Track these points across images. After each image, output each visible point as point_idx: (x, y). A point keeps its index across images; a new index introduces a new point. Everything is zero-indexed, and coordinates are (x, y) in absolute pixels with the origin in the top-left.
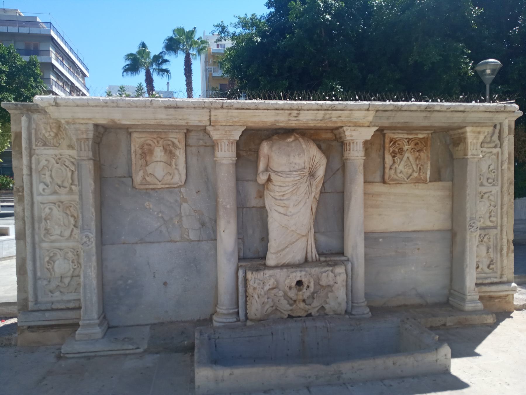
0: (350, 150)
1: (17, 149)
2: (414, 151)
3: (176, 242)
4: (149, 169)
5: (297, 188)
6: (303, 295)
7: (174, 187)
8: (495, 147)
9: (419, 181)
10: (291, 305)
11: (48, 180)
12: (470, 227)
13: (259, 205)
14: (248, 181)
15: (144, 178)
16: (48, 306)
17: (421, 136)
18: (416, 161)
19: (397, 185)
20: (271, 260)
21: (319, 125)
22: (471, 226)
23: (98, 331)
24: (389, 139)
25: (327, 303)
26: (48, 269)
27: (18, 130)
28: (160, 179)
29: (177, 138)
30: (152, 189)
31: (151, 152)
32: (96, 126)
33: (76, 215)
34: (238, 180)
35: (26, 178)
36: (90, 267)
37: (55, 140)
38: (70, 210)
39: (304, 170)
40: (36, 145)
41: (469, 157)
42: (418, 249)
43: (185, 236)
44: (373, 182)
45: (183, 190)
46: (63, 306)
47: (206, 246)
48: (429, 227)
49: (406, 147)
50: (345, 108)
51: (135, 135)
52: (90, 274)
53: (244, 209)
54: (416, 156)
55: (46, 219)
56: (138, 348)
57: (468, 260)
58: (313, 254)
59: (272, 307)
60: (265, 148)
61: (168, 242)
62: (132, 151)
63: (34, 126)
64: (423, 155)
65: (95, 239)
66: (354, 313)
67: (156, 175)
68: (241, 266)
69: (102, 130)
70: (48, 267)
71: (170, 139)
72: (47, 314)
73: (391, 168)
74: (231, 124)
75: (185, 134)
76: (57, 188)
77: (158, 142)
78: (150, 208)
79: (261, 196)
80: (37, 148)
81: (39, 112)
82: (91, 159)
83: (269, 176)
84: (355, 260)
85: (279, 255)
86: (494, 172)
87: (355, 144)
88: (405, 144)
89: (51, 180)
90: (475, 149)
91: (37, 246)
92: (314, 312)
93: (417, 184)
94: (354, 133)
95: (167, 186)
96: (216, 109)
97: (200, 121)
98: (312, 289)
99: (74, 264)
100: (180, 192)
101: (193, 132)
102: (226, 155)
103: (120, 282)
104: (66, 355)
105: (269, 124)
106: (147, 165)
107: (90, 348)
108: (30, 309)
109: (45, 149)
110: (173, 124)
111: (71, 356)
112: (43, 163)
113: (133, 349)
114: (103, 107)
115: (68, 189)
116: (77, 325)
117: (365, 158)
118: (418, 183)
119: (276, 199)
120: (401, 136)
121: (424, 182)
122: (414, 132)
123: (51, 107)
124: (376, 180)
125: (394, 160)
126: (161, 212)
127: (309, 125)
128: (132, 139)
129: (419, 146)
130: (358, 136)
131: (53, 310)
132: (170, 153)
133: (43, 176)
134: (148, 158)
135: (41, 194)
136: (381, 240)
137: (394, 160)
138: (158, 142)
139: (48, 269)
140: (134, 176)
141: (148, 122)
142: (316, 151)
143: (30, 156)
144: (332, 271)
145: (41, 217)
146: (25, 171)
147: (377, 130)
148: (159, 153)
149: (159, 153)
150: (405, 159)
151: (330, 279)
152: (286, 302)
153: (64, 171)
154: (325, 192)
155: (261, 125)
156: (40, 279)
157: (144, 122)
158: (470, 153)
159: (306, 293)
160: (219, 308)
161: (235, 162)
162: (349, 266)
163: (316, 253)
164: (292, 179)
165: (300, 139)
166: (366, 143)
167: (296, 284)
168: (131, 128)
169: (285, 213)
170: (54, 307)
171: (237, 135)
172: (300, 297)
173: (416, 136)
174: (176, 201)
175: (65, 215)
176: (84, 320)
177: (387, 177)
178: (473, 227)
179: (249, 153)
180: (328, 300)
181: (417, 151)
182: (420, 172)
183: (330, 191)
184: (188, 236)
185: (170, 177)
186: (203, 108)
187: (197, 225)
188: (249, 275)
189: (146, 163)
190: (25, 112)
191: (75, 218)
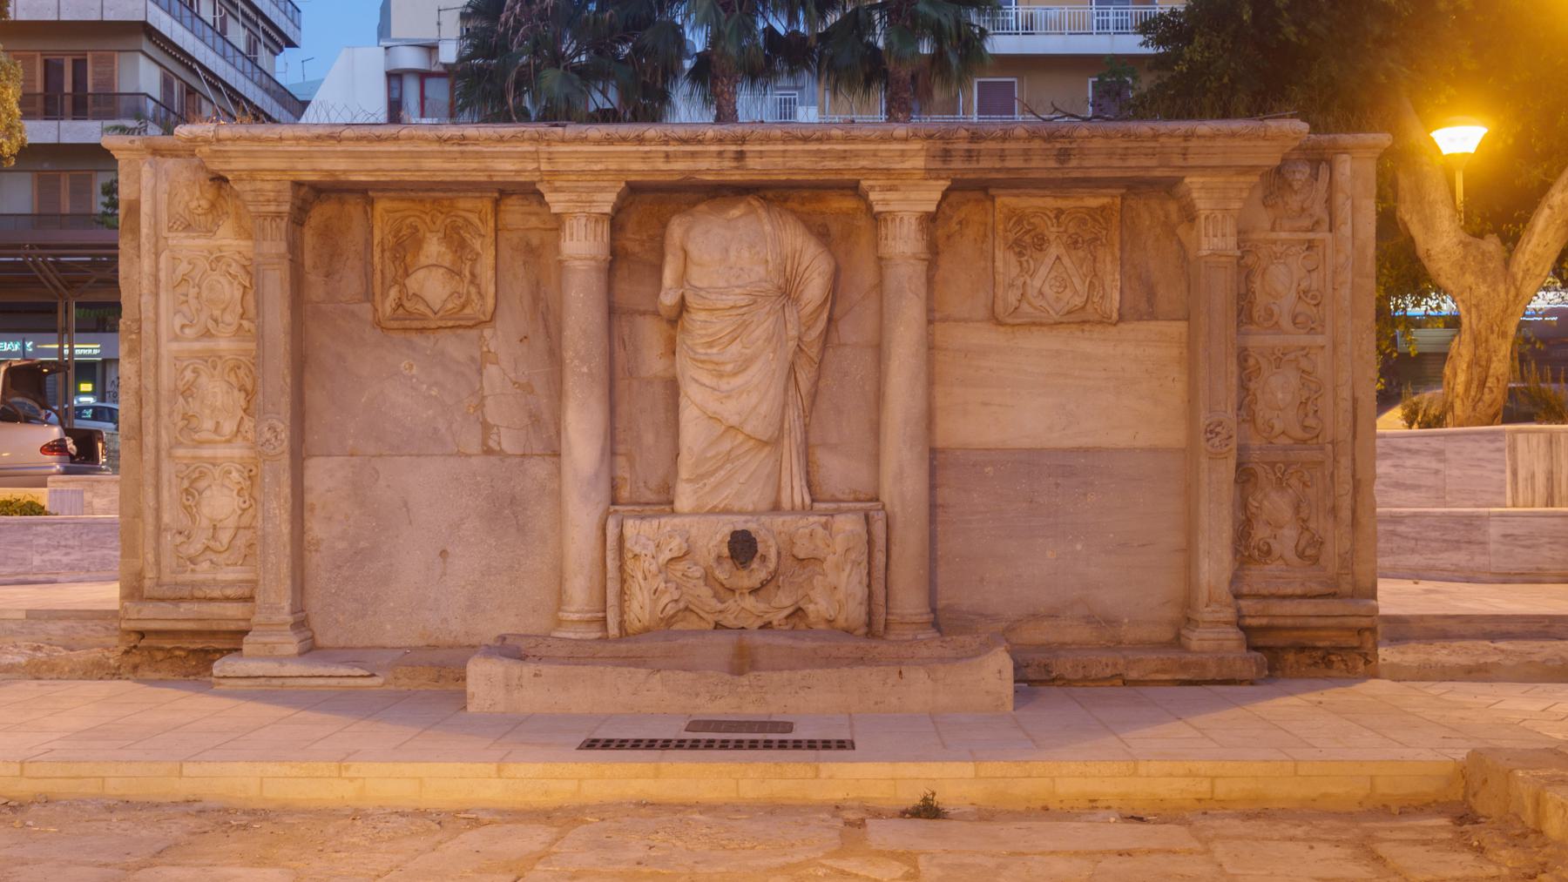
4: (413, 284)
14: (644, 313)
15: (400, 305)
19: (1034, 328)
21: (737, 178)
27: (133, 197)
28: (436, 308)
31: (418, 243)
32: (297, 184)
33: (249, 387)
34: (613, 312)
35: (146, 300)
37: (210, 217)
40: (170, 229)
44: (966, 321)
45: (487, 332)
47: (540, 469)
49: (1052, 232)
56: (373, 675)
59: (676, 601)
72: (184, 607)
91: (163, 454)
92: (777, 618)
98: (772, 565)
102: (582, 245)
103: (341, 545)
116: (246, 633)
121: (1104, 321)
125: (1021, 264)
132: (457, 241)
134: (408, 259)
135: (176, 338)
143: (157, 255)
148: (434, 248)
149: (434, 248)
151: (820, 543)
153: (227, 286)
171: (606, 202)
174: (473, 359)
177: (999, 308)
188: (631, 527)
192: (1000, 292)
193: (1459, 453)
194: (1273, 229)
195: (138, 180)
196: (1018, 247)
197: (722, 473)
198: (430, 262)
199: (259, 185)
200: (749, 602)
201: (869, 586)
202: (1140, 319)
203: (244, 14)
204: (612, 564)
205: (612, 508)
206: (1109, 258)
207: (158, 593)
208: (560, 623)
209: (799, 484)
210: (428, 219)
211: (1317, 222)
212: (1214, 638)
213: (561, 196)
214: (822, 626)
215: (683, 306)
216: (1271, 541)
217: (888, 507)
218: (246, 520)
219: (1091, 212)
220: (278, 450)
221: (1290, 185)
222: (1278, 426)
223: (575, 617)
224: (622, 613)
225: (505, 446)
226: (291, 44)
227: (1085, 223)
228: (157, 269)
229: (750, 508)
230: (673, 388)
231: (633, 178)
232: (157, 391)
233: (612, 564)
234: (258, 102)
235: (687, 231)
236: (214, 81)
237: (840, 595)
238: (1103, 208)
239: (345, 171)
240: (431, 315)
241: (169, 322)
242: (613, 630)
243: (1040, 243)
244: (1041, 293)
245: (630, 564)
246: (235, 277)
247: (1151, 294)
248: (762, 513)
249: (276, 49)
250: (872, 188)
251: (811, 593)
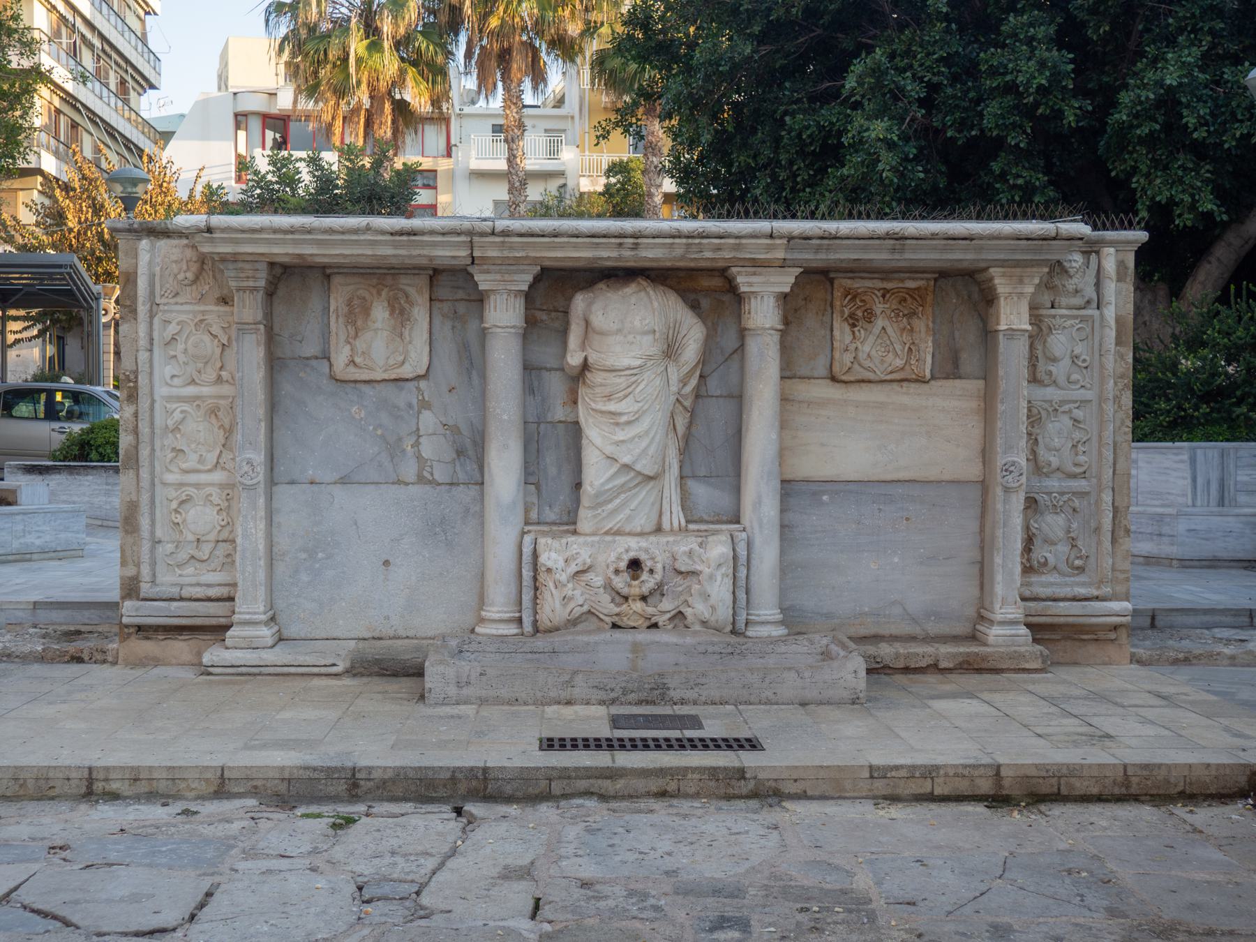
4: (360, 344)
16: (175, 591)
19: (863, 385)
42: (907, 519)
43: (426, 474)
61: (393, 483)
64: (920, 324)
66: (749, 633)
68: (529, 532)
69: (279, 271)
75: (431, 277)
80: (163, 300)
98: (658, 576)
100: (418, 388)
108: (142, 595)
116: (227, 627)
121: (921, 380)
122: (896, 275)
131: (181, 599)
132: (400, 313)
134: (359, 323)
140: (333, 355)
150: (877, 330)
154: (708, 396)
156: (159, 542)
159: (648, 582)
165: (649, 289)
170: (185, 593)
171: (524, 281)
172: (635, 591)
173: (901, 285)
177: (836, 369)
179: (553, 314)
183: (718, 393)
187: (449, 455)
192: (837, 355)
193: (1148, 463)
196: (853, 321)
197: (618, 501)
199: (240, 265)
200: (638, 606)
201: (734, 593)
202: (947, 378)
203: (116, 63)
206: (923, 329)
208: (482, 620)
209: (677, 508)
211: (1088, 302)
212: (1006, 633)
213: (488, 277)
215: (585, 366)
217: (748, 529)
218: (225, 535)
219: (909, 291)
220: (255, 481)
221: (1066, 272)
223: (497, 616)
225: (437, 476)
226: (152, 87)
227: (905, 300)
229: (639, 529)
230: (575, 431)
233: (527, 573)
234: (128, 135)
235: (590, 305)
236: (94, 117)
237: (712, 601)
238: (918, 289)
239: (311, 255)
242: (528, 627)
243: (869, 316)
245: (542, 577)
246: (215, 337)
247: (956, 362)
248: (649, 534)
249: (140, 91)
250: (739, 273)
251: (690, 599)
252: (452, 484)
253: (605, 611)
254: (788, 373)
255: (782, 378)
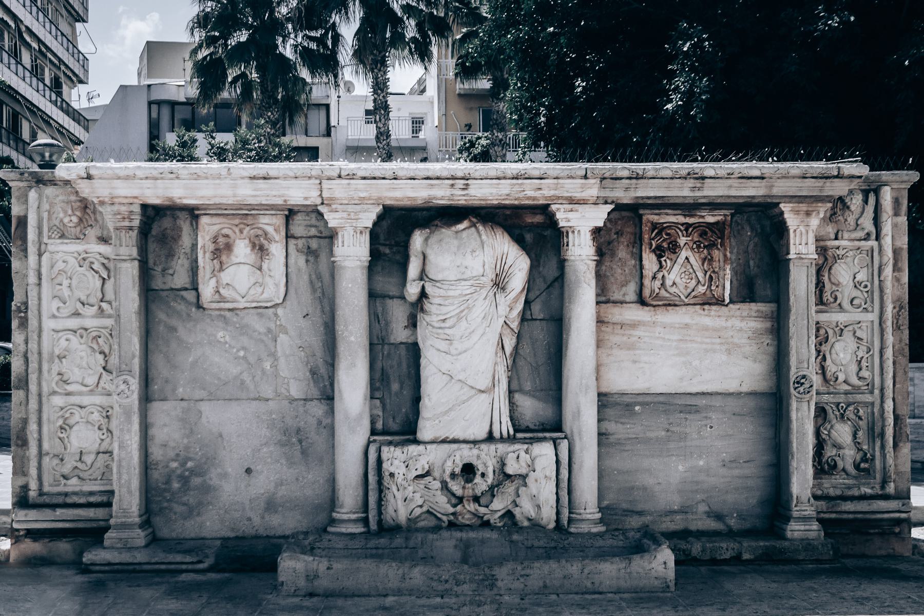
0: (568, 245)
1: (20, 243)
2: (699, 247)
3: (267, 400)
5: (468, 308)
6: (473, 489)
7: (267, 307)
8: (867, 237)
9: (711, 301)
10: (455, 506)
11: (66, 293)
12: (796, 385)
13: (410, 341)
14: (392, 298)
17: (711, 219)
18: (703, 265)
20: (426, 431)
22: (798, 383)
23: (139, 537)
24: (649, 224)
25: (517, 506)
26: (60, 438)
27: (22, 214)
29: (271, 224)
30: (229, 310)
31: (229, 247)
32: (144, 207)
33: (107, 351)
36: (129, 431)
37: (78, 229)
38: (98, 343)
39: (482, 278)
40: (49, 238)
41: (790, 256)
44: (622, 303)
45: (280, 311)
46: (82, 500)
48: (732, 386)
49: (682, 241)
50: (545, 176)
51: (204, 220)
52: (129, 442)
53: (386, 347)
54: (703, 256)
55: (60, 358)
56: (200, 562)
57: (795, 445)
58: (505, 426)
59: (421, 506)
60: (417, 239)
62: (199, 247)
63: (46, 206)
65: (138, 386)
67: (237, 287)
68: (375, 441)
69: (150, 212)
70: (61, 436)
71: (261, 226)
72: (59, 512)
73: (654, 278)
74: (356, 202)
76: (79, 305)
77: (241, 231)
78: (226, 343)
79: (413, 323)
81: (55, 185)
82: (135, 259)
83: (423, 287)
84: (576, 438)
85: (437, 422)
86: (866, 286)
87: (576, 232)
88: (680, 233)
89: (70, 293)
90: (803, 244)
92: (494, 519)
93: (706, 307)
94: (570, 215)
95: (254, 305)
96: (329, 179)
97: (306, 199)
98: (490, 479)
99: (101, 432)
100: (276, 315)
101: (299, 214)
102: (353, 252)
103: (174, 465)
104: (91, 567)
105: (420, 202)
106: (221, 269)
107: (125, 557)
109: (62, 243)
110: (264, 202)
111: (97, 568)
112: (60, 265)
113: (192, 563)
114: (156, 179)
115: (96, 308)
117: (596, 258)
118: (710, 304)
119: (433, 327)
120: (672, 219)
121: (720, 302)
123: (80, 181)
124: (628, 299)
125: (660, 263)
126: (244, 348)
127: (489, 202)
128: (200, 227)
129: (709, 238)
130: (581, 224)
132: (260, 250)
133: (58, 287)
134: (224, 258)
135: (54, 316)
136: (637, 408)
137: (660, 263)
138: (241, 231)
139: (60, 438)
140: (201, 287)
141: (224, 201)
142: (507, 245)
143: (40, 255)
144: (527, 452)
145: (53, 352)
146: (32, 279)
147: (612, 210)
148: (242, 250)
149: (242, 250)
150: (681, 259)
152: (445, 499)
154: (533, 319)
155: (407, 203)
157: (217, 201)
158: (793, 250)
159: (481, 485)
160: (338, 513)
161: (367, 264)
162: (564, 446)
163: (510, 423)
164: (459, 292)
166: (596, 232)
167: (462, 470)
168: (198, 209)
169: (446, 350)
170: (69, 500)
171: (369, 218)
172: (469, 492)
173: (701, 220)
174: (269, 331)
175: (89, 351)
176: (117, 517)
177: (646, 293)
178: (802, 384)
180: (518, 500)
181: (705, 247)
182: (710, 286)
184: (288, 391)
185: (260, 290)
186: (310, 178)
188: (387, 452)
189: (221, 267)
190: (34, 184)
191: (106, 356)
194: (836, 238)
195: (26, 201)
196: (659, 252)
198: (238, 261)
201: (557, 493)
204: (372, 478)
205: (372, 438)
207: (41, 500)
210: (237, 230)
214: (526, 524)
216: (837, 458)
217: (569, 436)
221: (848, 208)
222: (842, 377)
224: (380, 513)
228: (40, 265)
231: (388, 202)
232: (40, 353)
233: (372, 478)
238: (717, 223)
240: (240, 299)
241: (49, 305)
242: (373, 526)
244: (674, 283)
252: (305, 400)
253: (442, 511)
254: (603, 298)
255: (598, 303)
